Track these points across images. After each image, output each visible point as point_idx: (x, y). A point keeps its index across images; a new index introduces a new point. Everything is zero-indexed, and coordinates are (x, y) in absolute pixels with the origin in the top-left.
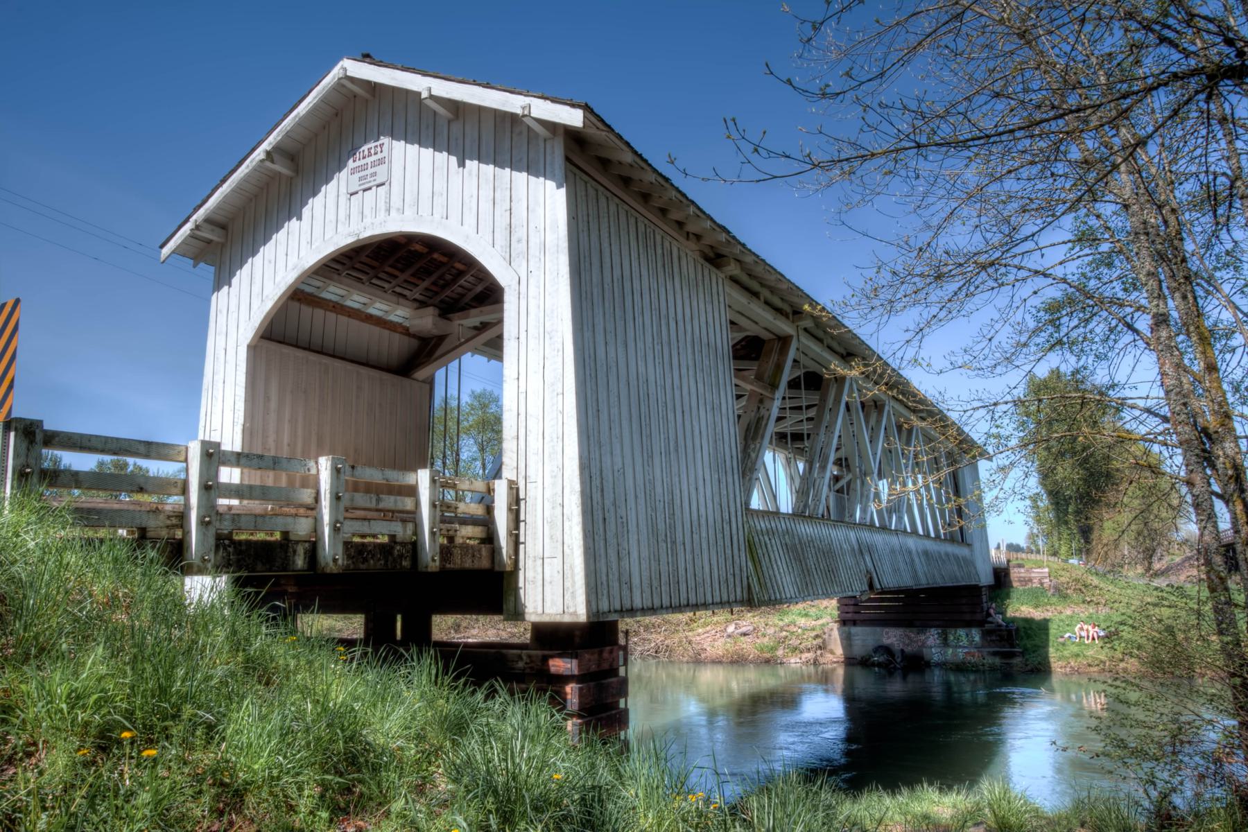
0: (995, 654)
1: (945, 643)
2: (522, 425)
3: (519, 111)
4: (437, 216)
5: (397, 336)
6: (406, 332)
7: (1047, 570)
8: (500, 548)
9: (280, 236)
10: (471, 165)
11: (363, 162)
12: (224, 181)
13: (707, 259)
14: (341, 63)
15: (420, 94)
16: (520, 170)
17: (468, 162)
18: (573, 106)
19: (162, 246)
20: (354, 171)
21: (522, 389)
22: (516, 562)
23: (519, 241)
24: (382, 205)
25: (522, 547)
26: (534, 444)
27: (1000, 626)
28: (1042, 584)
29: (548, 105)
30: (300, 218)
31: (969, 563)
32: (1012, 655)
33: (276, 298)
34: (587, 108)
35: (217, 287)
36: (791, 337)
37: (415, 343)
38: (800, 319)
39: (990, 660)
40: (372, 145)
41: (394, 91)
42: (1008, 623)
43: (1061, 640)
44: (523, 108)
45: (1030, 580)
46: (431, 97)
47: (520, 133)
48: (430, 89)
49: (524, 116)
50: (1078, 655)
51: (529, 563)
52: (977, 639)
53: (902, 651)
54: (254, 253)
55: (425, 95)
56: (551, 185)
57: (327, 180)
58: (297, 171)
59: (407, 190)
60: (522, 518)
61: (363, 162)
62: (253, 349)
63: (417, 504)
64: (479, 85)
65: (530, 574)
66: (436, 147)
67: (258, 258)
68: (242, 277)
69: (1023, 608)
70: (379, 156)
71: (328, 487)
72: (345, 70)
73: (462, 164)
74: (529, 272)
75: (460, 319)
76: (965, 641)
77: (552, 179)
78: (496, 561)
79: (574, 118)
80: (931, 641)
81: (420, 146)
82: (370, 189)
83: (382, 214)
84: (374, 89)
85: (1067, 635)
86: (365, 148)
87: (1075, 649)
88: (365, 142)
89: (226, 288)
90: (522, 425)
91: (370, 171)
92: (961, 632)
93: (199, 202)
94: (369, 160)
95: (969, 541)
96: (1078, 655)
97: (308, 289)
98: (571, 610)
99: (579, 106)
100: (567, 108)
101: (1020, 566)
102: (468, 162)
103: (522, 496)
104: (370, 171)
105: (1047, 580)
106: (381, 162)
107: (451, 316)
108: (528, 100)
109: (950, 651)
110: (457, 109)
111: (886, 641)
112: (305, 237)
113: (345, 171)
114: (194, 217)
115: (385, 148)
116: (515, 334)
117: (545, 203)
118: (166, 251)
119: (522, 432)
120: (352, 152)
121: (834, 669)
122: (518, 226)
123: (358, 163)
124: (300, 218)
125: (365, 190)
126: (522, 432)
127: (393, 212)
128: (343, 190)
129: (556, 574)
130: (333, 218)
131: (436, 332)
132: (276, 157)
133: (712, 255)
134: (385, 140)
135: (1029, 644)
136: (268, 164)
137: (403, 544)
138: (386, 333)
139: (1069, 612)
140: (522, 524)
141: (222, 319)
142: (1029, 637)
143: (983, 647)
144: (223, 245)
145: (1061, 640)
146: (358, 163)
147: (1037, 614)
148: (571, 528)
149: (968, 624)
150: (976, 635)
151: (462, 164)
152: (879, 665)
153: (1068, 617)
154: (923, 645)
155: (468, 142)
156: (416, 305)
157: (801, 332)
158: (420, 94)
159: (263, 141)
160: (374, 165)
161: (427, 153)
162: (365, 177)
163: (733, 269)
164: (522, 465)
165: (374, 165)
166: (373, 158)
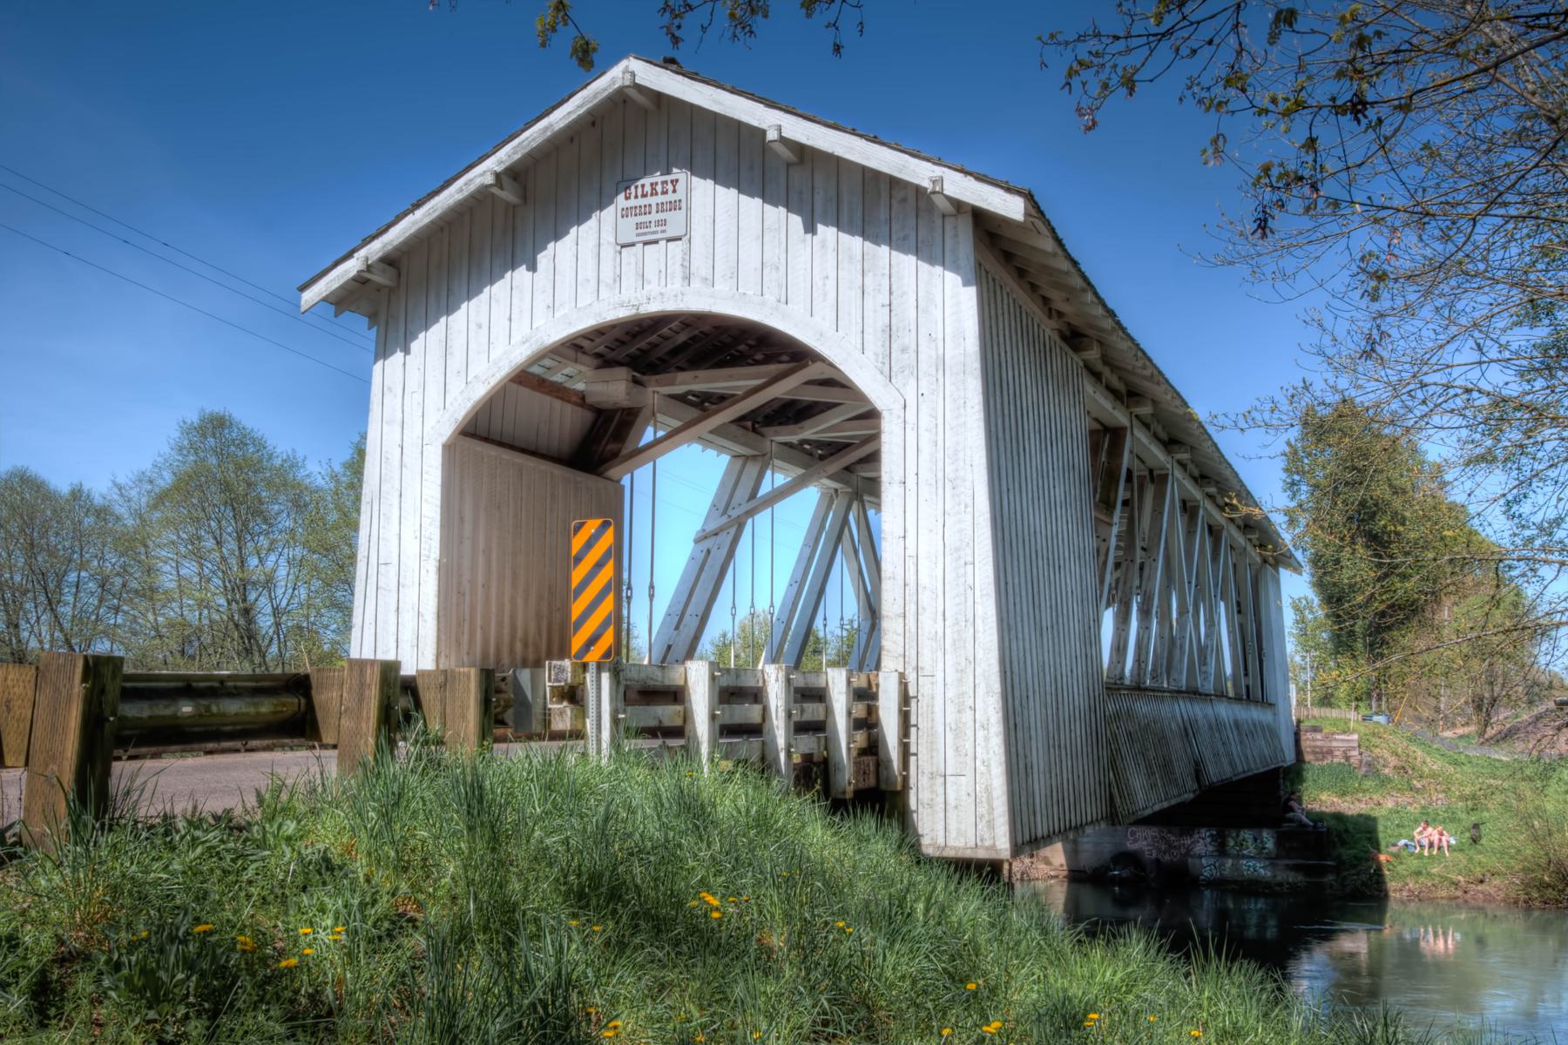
0: (1296, 868)
1: (1222, 851)
2: (911, 599)
3: (926, 184)
4: (770, 298)
5: (569, 408)
6: (581, 400)
7: (1356, 737)
8: (890, 761)
9: (499, 289)
10: (826, 232)
11: (641, 202)
12: (417, 206)
13: (1064, 338)
14: (623, 64)
15: (764, 132)
16: (905, 251)
17: (820, 227)
18: (1009, 190)
19: (303, 288)
20: (626, 213)
21: (911, 551)
22: (906, 779)
23: (904, 350)
24: (676, 269)
25: (913, 759)
26: (929, 625)
27: (1305, 826)
28: (1347, 758)
29: (970, 182)
30: (533, 267)
31: (1271, 732)
32: (1323, 870)
33: (493, 382)
34: (1029, 197)
35: (383, 352)
36: (1124, 429)
37: (589, 416)
38: (1138, 404)
39: (1292, 877)
40: (658, 178)
41: (738, 127)
42: (1315, 822)
43: (1394, 849)
44: (934, 182)
45: (1330, 752)
46: (783, 140)
47: (904, 200)
48: (779, 128)
49: (934, 192)
50: (1418, 873)
51: (924, 781)
52: (1270, 845)
53: (1157, 860)
54: (450, 309)
55: (772, 135)
56: (953, 279)
57: (580, 219)
58: (525, 198)
59: (714, 252)
60: (913, 721)
61: (641, 202)
62: (449, 448)
63: (829, 711)
64: (861, 136)
65: (925, 795)
66: (768, 197)
67: (458, 319)
68: (428, 342)
69: (1324, 797)
70: (670, 197)
71: (781, 703)
72: (633, 74)
73: (810, 228)
74: (920, 395)
75: (659, 384)
76: (1251, 849)
77: (956, 269)
78: (883, 774)
79: (1011, 207)
80: (1199, 848)
81: (764, 201)
82: (656, 242)
83: (676, 284)
84: (659, 98)
85: (1402, 842)
86: (647, 181)
87: (1414, 864)
88: (645, 174)
89: (399, 355)
90: (911, 599)
91: (654, 217)
92: (1247, 835)
93: (374, 231)
94: (653, 200)
95: (1272, 700)
96: (1418, 873)
97: (536, 370)
98: (987, 843)
99: (1019, 192)
100: (1000, 192)
101: (1316, 729)
102: (820, 227)
103: (912, 692)
104: (654, 217)
105: (1355, 753)
106: (675, 206)
107: (765, 430)
108: (938, 171)
109: (1230, 862)
110: (804, 154)
111: (1132, 846)
112: (542, 300)
113: (611, 209)
114: (362, 253)
115: (680, 186)
116: (898, 476)
117: (945, 307)
118: (310, 296)
119: (911, 608)
120: (624, 184)
121: (1048, 889)
122: (908, 339)
123: (632, 202)
124: (533, 267)
125: (645, 243)
126: (911, 608)
127: (696, 283)
128: (608, 237)
129: (965, 797)
130: (592, 276)
131: (626, 403)
132: (506, 180)
133: (1068, 333)
134: (679, 174)
135: (1346, 853)
136: (495, 190)
137: (817, 764)
138: (558, 404)
139: (1390, 804)
140: (913, 730)
141: (393, 402)
142: (1343, 843)
143: (1278, 857)
144: (391, 290)
145: (1394, 849)
146: (632, 202)
147: (1351, 806)
148: (987, 739)
149: (1256, 824)
150: (1269, 840)
151: (810, 228)
152: (1121, 882)
153: (1391, 811)
154: (1188, 853)
155: (817, 198)
156: (596, 362)
157: (1135, 421)
158: (764, 132)
159: (487, 156)
160: (661, 208)
161: (752, 205)
162: (647, 225)
163: (1093, 354)
164: (911, 653)
165: (661, 208)
166: (660, 199)
